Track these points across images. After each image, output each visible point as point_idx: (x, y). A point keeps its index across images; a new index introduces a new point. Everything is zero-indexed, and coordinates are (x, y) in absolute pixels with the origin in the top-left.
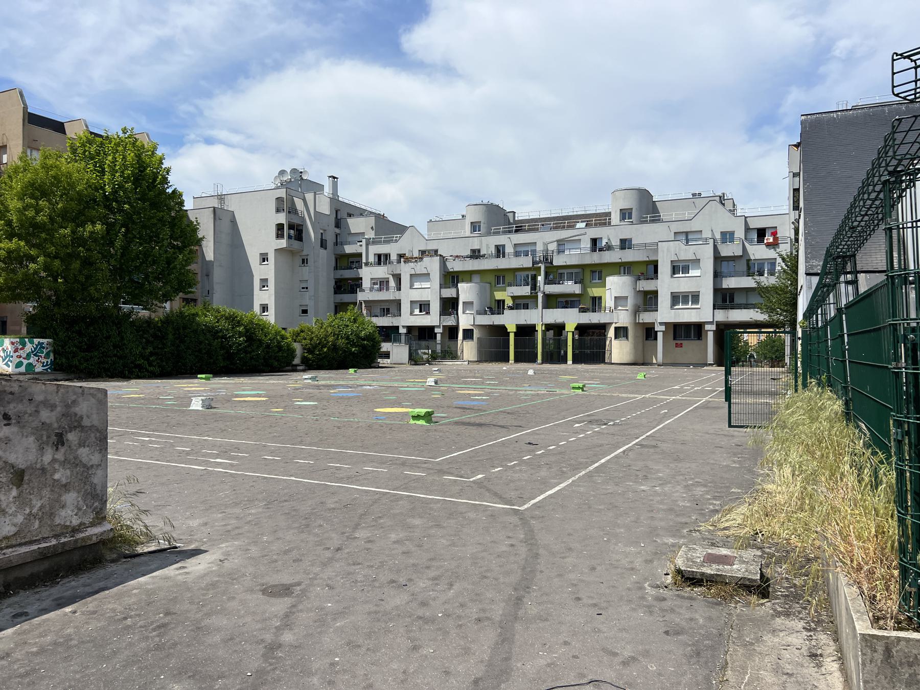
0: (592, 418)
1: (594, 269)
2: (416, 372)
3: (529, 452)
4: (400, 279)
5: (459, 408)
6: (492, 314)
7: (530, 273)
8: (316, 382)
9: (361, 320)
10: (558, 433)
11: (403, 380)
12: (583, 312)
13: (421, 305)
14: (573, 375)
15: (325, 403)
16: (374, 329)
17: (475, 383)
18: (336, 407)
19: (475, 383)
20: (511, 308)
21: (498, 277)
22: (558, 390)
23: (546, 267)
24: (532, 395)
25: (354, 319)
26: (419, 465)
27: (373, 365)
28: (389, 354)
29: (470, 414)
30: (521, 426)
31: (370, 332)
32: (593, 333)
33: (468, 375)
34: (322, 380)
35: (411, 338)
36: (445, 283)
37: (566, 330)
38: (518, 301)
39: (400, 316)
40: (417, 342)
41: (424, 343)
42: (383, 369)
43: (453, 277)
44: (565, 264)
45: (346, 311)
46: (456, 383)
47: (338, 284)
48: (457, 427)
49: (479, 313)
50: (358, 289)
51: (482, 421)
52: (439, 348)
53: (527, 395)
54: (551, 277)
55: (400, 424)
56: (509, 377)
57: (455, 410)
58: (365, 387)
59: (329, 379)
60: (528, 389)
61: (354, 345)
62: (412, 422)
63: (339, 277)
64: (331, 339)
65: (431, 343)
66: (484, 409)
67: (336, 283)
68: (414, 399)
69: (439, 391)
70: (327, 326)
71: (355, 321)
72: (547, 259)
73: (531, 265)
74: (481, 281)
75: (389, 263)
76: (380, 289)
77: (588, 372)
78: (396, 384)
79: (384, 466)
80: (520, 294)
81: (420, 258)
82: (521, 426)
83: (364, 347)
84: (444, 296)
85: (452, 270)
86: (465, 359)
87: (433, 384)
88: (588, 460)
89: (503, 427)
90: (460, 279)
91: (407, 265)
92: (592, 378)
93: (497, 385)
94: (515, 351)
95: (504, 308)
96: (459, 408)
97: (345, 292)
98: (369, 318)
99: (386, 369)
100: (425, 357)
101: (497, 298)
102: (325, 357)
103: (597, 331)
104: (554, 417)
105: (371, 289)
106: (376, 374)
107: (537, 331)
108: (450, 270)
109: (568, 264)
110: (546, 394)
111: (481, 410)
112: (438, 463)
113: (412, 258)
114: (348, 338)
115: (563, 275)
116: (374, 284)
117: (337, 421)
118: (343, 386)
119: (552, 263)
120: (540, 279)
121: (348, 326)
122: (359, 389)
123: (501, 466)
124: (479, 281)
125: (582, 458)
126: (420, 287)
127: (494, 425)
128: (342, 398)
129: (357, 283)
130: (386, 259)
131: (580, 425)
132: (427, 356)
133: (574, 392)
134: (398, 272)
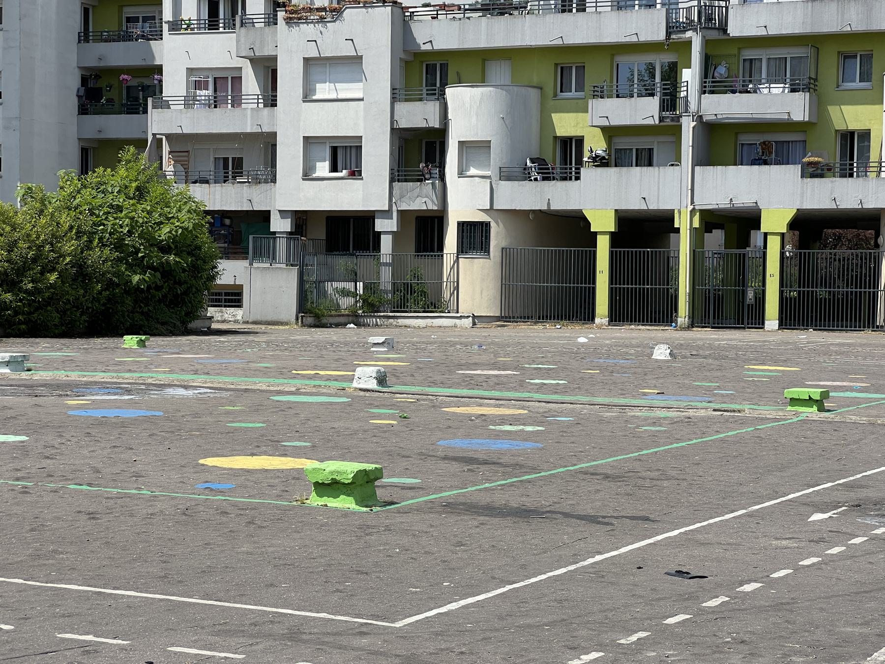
0: (863, 494)
1: (847, 48)
2: (320, 346)
3: (686, 601)
4: (274, 72)
5: (455, 459)
6: (544, 179)
7: (660, 60)
8: (24, 375)
9: (160, 190)
10: (763, 542)
11: (281, 373)
12: (813, 176)
13: (334, 150)
14: (785, 362)
15: (50, 438)
16: (196, 219)
17: (499, 383)
18: (85, 452)
19: (499, 383)
20: (601, 162)
21: (564, 71)
22: (746, 407)
23: (707, 43)
24: (673, 422)
25: (138, 189)
26: (344, 641)
27: (193, 325)
28: (240, 294)
29: (488, 480)
30: (646, 519)
31: (185, 229)
32: (839, 238)
33: (476, 359)
34: (45, 369)
35: (304, 246)
36: (407, 87)
37: (764, 229)
38: (623, 143)
39: (274, 180)
40: (322, 257)
41: (341, 262)
42: (222, 338)
43: (430, 70)
44: (762, 32)
45: (113, 164)
46: (443, 384)
47: (91, 85)
48: (452, 519)
49: (506, 175)
50: (150, 100)
51: (529, 503)
52: (386, 277)
53: (656, 422)
54: (722, 70)
55: (277, 507)
56: (599, 367)
57: (443, 465)
58: (170, 391)
59: (66, 363)
60: (656, 403)
61: (139, 265)
62: (315, 501)
63: (92, 63)
64: (69, 246)
65: (363, 262)
66: (530, 463)
67: (84, 80)
68: (318, 430)
69: (392, 406)
70: (58, 209)
71: (141, 193)
72: (710, 19)
73: (661, 36)
74: (516, 81)
75: (242, 24)
76: (216, 103)
77: (828, 353)
78: (261, 384)
79: (233, 641)
80: (627, 122)
81: (334, 10)
82: (646, 519)
83: (166, 271)
84: (403, 124)
85: (428, 47)
86: (464, 309)
87: (373, 384)
88: (866, 630)
89: (592, 519)
90: (451, 75)
91: (295, 30)
92: (844, 373)
93: (564, 390)
94: (611, 290)
95: (580, 162)
96: (455, 459)
97: (110, 109)
98: (182, 186)
99: (230, 338)
100: (346, 302)
101: (561, 132)
102: (50, 298)
103: (850, 233)
104: (744, 489)
105: (189, 102)
106: (201, 350)
107: (678, 231)
108: (424, 48)
109: (773, 31)
110: (714, 417)
111: (521, 466)
112: (403, 635)
113: (310, 10)
114: (119, 246)
115: (756, 65)
116: (198, 85)
117: (87, 494)
118: (104, 387)
119: (725, 31)
120: (690, 76)
121: (119, 209)
122: (155, 395)
123: (600, 647)
124: (508, 82)
125: (847, 623)
126: (333, 96)
127: (566, 515)
128: (102, 423)
129: (147, 82)
130: (234, 13)
131: (826, 516)
132: (351, 300)
133: (797, 414)
134: (268, 52)
